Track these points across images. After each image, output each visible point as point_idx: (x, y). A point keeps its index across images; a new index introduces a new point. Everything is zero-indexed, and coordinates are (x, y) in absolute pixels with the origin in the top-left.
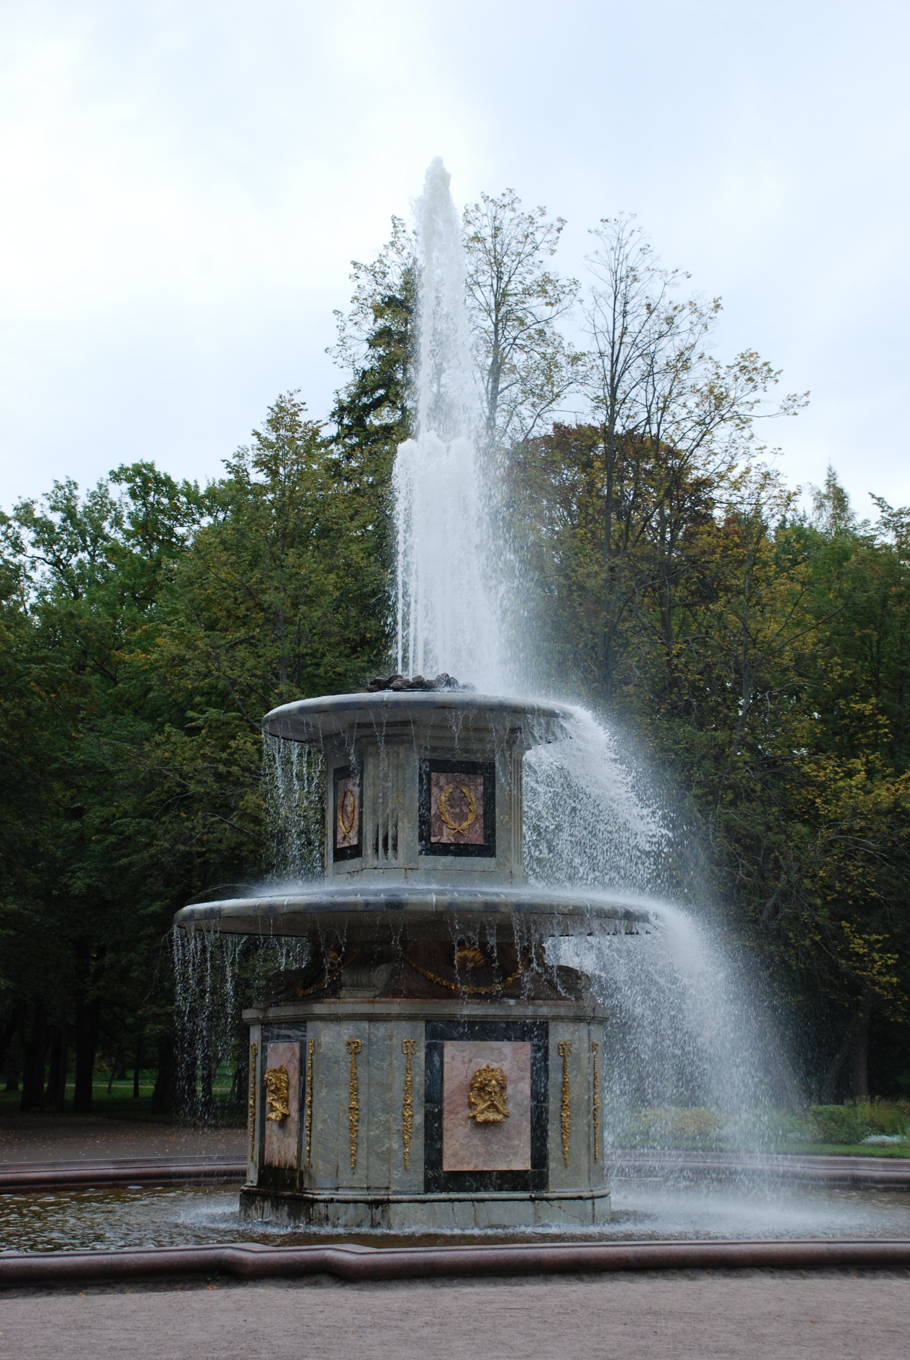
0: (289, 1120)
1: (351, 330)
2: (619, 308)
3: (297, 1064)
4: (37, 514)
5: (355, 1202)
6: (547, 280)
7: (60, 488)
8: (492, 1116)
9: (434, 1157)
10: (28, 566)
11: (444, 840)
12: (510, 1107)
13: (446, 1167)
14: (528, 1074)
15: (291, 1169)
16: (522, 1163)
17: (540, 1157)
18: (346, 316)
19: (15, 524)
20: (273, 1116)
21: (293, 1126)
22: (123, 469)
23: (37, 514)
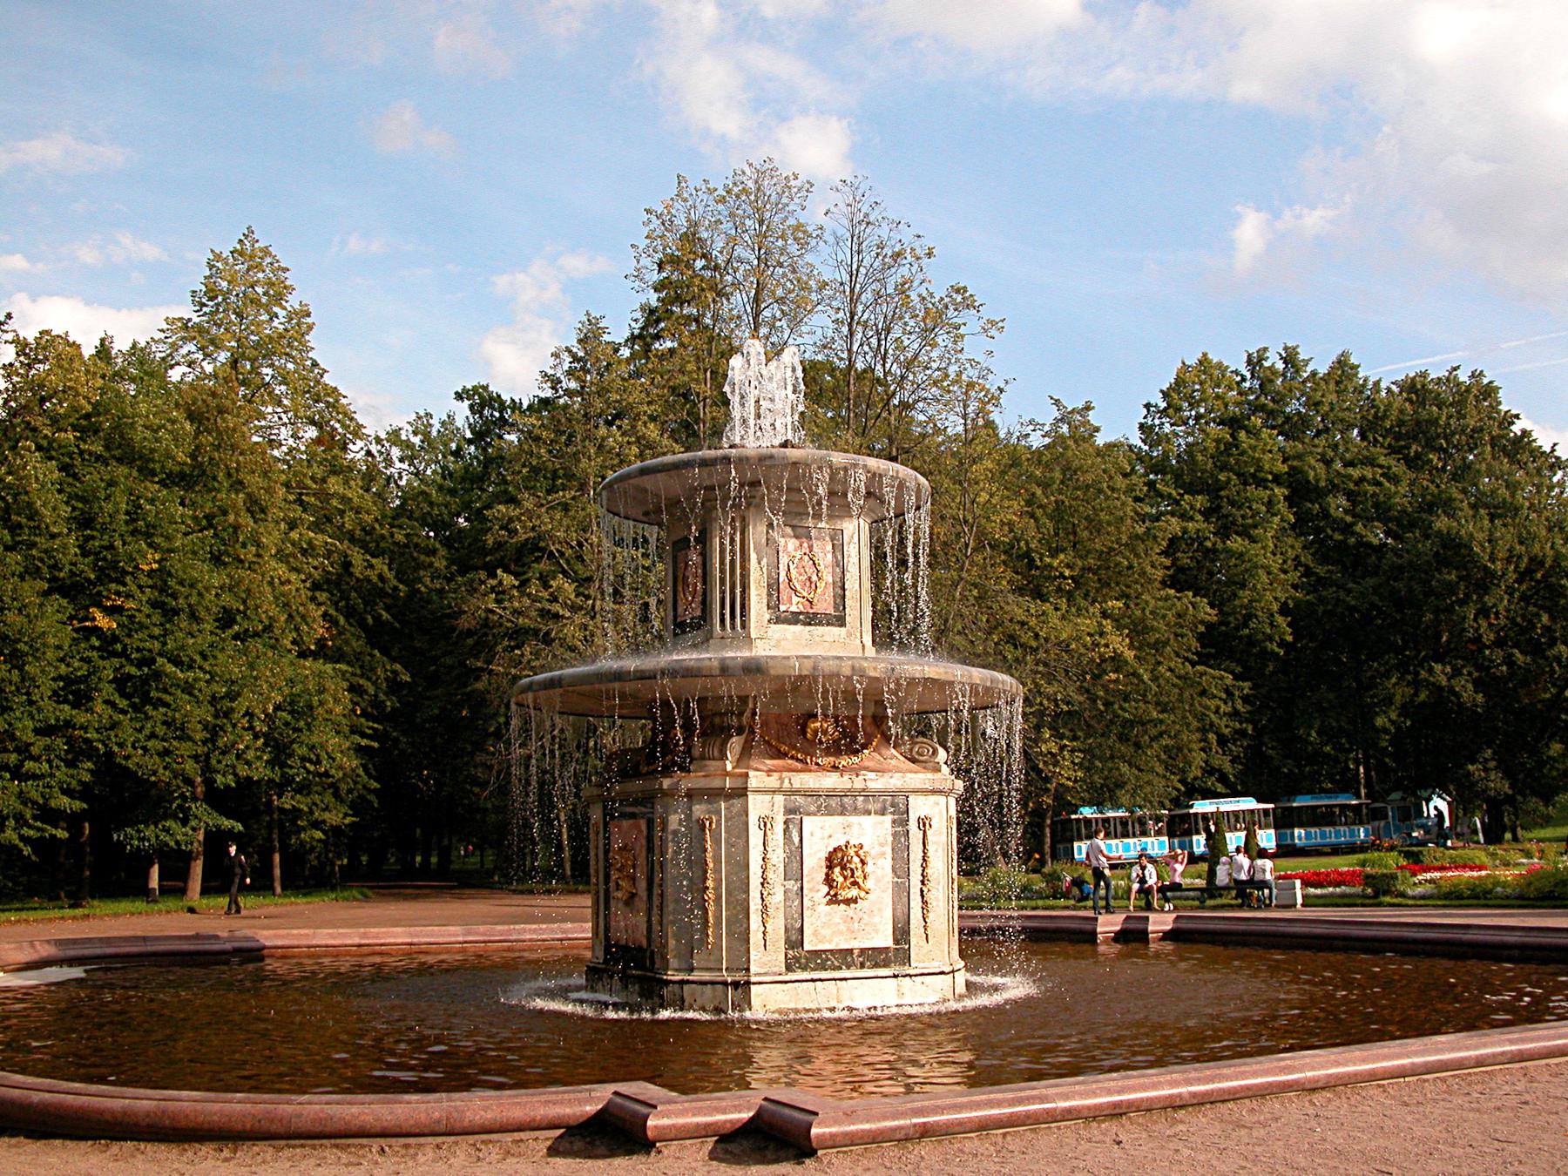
0: (637, 899)
1: (645, 261)
2: (855, 248)
3: (644, 842)
4: (404, 437)
5: (713, 983)
6: (799, 227)
7: (420, 418)
8: (854, 892)
9: (795, 940)
10: (396, 476)
11: (794, 609)
12: (869, 884)
13: (807, 947)
14: (888, 850)
15: (640, 948)
16: (883, 938)
17: (902, 933)
18: (640, 250)
19: (387, 445)
20: (619, 894)
21: (641, 904)
22: (465, 390)
23: (404, 437)
